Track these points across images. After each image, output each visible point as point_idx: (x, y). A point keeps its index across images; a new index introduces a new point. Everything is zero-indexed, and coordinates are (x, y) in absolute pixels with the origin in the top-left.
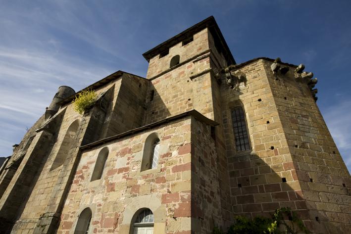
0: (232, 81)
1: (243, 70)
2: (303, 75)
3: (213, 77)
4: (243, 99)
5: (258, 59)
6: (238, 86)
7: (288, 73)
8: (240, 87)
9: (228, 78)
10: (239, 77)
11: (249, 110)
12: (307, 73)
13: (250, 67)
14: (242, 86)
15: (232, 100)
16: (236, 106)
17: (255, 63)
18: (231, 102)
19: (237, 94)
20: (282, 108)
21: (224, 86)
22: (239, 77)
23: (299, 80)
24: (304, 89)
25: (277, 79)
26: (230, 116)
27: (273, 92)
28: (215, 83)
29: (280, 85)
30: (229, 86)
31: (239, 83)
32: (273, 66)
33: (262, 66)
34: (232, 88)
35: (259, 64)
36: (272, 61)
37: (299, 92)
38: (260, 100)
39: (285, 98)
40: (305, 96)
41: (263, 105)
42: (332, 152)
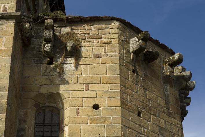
0: (54, 47)
1: (79, 31)
2: (177, 70)
3: (19, 31)
4: (66, 96)
5: (113, 19)
6: (63, 63)
7: (155, 61)
8: (65, 66)
9: (48, 41)
10: (69, 45)
11: (71, 122)
12: (183, 70)
13: (93, 29)
14: (69, 65)
15: (44, 90)
16: (47, 104)
17: (104, 26)
18: (41, 94)
19: (57, 80)
20: (130, 133)
21: (35, 52)
22: (69, 45)
23: (169, 80)
24: (172, 100)
25: (134, 71)
26: (33, 123)
27: (122, 97)
28: (19, 44)
29: (137, 84)
30: (45, 56)
31: (66, 57)
32: (134, 43)
33: (116, 36)
34: (50, 63)
35: (112, 31)
36: (136, 31)
37: (163, 104)
38: (96, 107)
39: (139, 114)
40: (169, 115)
41: (98, 120)
42: (132, 70)
